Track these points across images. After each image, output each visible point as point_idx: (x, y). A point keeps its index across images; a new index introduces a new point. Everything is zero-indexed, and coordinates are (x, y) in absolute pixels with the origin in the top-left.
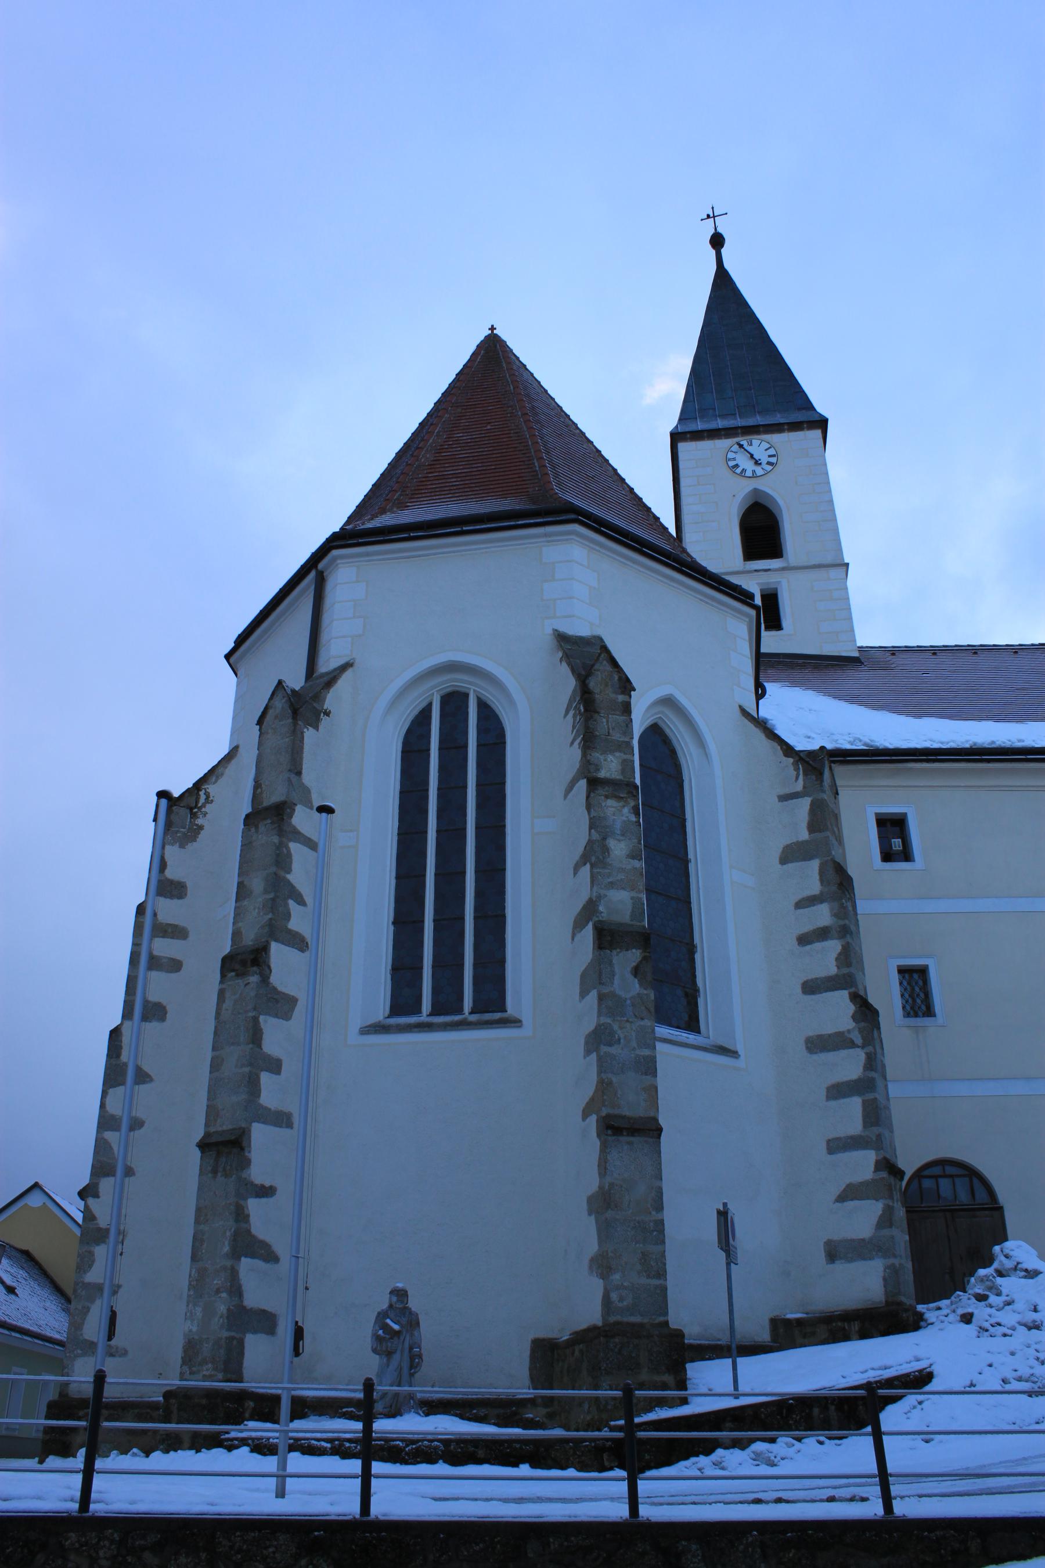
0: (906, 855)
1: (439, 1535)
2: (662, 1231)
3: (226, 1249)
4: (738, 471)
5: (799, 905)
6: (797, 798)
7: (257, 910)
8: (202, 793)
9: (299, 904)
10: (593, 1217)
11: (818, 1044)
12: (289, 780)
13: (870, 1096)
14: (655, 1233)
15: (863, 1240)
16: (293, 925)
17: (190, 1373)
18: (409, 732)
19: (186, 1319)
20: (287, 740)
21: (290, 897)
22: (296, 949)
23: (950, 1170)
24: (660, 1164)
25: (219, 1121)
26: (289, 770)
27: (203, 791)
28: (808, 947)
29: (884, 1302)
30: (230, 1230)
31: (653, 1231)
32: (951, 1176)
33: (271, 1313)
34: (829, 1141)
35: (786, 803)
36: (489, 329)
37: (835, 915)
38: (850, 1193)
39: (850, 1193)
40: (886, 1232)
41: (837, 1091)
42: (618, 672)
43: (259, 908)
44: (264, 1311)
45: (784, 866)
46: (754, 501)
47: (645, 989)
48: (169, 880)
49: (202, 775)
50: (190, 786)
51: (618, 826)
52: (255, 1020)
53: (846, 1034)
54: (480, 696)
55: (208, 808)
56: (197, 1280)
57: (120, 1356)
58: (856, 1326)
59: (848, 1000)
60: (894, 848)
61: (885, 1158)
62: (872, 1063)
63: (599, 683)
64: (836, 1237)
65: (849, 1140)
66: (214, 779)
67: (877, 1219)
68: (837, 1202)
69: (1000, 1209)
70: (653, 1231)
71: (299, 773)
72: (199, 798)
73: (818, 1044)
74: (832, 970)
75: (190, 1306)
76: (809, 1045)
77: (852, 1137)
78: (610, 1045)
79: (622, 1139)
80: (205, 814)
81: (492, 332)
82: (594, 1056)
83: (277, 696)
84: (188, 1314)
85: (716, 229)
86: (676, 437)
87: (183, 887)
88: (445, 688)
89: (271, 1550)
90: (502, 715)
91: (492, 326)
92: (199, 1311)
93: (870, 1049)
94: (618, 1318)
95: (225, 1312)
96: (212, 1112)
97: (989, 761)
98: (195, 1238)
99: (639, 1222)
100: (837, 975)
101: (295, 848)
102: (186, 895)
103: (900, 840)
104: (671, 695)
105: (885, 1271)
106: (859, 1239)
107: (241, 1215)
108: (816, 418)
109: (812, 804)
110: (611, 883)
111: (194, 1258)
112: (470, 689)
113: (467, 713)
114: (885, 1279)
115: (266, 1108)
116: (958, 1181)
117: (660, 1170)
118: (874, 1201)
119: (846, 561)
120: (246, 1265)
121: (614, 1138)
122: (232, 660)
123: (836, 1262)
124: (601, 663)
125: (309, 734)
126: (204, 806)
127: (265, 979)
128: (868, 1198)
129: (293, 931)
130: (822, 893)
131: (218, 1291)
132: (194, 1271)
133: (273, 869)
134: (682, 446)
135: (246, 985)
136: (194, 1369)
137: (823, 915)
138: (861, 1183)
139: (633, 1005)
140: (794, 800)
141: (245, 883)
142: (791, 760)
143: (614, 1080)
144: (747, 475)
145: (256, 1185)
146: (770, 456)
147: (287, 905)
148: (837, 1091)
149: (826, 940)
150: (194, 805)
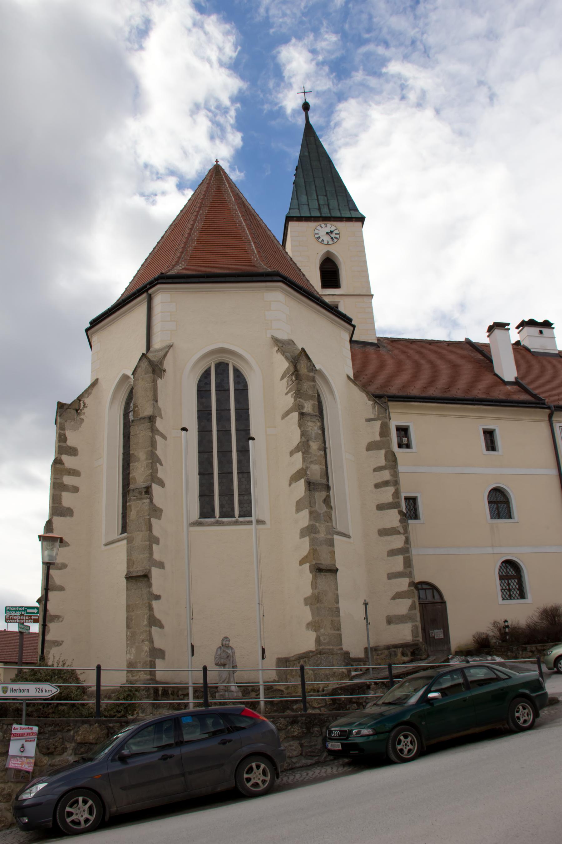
0: (408, 446)
2: (339, 612)
3: (145, 623)
4: (320, 240)
5: (375, 470)
6: (374, 421)
7: (143, 468)
8: (81, 402)
11: (383, 532)
12: (154, 405)
13: (407, 555)
15: (403, 615)
17: (132, 676)
18: (200, 381)
19: (127, 654)
20: (150, 384)
23: (425, 586)
24: (337, 584)
25: (134, 566)
26: (153, 400)
27: (82, 401)
28: (379, 489)
30: (147, 614)
31: (335, 612)
32: (425, 589)
34: (388, 574)
35: (369, 422)
36: (215, 161)
37: (392, 476)
38: (398, 596)
39: (398, 596)
40: (413, 612)
41: (392, 553)
42: (310, 361)
43: (144, 467)
44: (161, 649)
45: (369, 452)
46: (327, 257)
47: (328, 509)
49: (81, 393)
50: (75, 398)
51: (313, 435)
52: (149, 520)
54: (234, 365)
55: (85, 410)
56: (131, 637)
58: (400, 650)
59: (397, 514)
60: (404, 442)
61: (413, 581)
62: (407, 541)
63: (303, 369)
64: (391, 614)
66: (87, 395)
69: (443, 603)
70: (335, 612)
71: (157, 401)
72: (80, 405)
73: (383, 532)
74: (390, 500)
75: (129, 648)
76: (380, 533)
77: (399, 573)
78: (315, 533)
79: (322, 573)
80: (84, 413)
81: (217, 163)
82: (307, 539)
83: (142, 361)
84: (128, 651)
85: (305, 100)
86: (289, 219)
87: (76, 450)
88: (216, 360)
89: (279, 724)
90: (246, 374)
91: (217, 160)
92: (133, 650)
93: (406, 535)
94: (323, 647)
95: (148, 650)
96: (130, 562)
97: (447, 403)
98: (127, 618)
99: (330, 608)
100: (392, 502)
101: (158, 438)
102: (78, 454)
104: (320, 369)
105: (412, 627)
106: (401, 615)
107: (151, 608)
108: (360, 216)
109: (382, 424)
110: (312, 461)
111: (128, 627)
112: (230, 361)
113: (228, 374)
114: (412, 631)
116: (427, 591)
117: (337, 586)
118: (408, 599)
119: (372, 293)
120: (154, 629)
121: (319, 573)
122: (89, 332)
124: (302, 357)
125: (159, 381)
127: (151, 500)
128: (405, 598)
130: (386, 465)
131: (143, 641)
133: (150, 448)
134: (291, 224)
136: (134, 674)
137: (386, 475)
138: (403, 592)
139: (324, 516)
140: (373, 422)
141: (135, 454)
142: (371, 403)
143: (318, 548)
144: (324, 243)
147: (156, 466)
148: (392, 553)
150: (78, 409)
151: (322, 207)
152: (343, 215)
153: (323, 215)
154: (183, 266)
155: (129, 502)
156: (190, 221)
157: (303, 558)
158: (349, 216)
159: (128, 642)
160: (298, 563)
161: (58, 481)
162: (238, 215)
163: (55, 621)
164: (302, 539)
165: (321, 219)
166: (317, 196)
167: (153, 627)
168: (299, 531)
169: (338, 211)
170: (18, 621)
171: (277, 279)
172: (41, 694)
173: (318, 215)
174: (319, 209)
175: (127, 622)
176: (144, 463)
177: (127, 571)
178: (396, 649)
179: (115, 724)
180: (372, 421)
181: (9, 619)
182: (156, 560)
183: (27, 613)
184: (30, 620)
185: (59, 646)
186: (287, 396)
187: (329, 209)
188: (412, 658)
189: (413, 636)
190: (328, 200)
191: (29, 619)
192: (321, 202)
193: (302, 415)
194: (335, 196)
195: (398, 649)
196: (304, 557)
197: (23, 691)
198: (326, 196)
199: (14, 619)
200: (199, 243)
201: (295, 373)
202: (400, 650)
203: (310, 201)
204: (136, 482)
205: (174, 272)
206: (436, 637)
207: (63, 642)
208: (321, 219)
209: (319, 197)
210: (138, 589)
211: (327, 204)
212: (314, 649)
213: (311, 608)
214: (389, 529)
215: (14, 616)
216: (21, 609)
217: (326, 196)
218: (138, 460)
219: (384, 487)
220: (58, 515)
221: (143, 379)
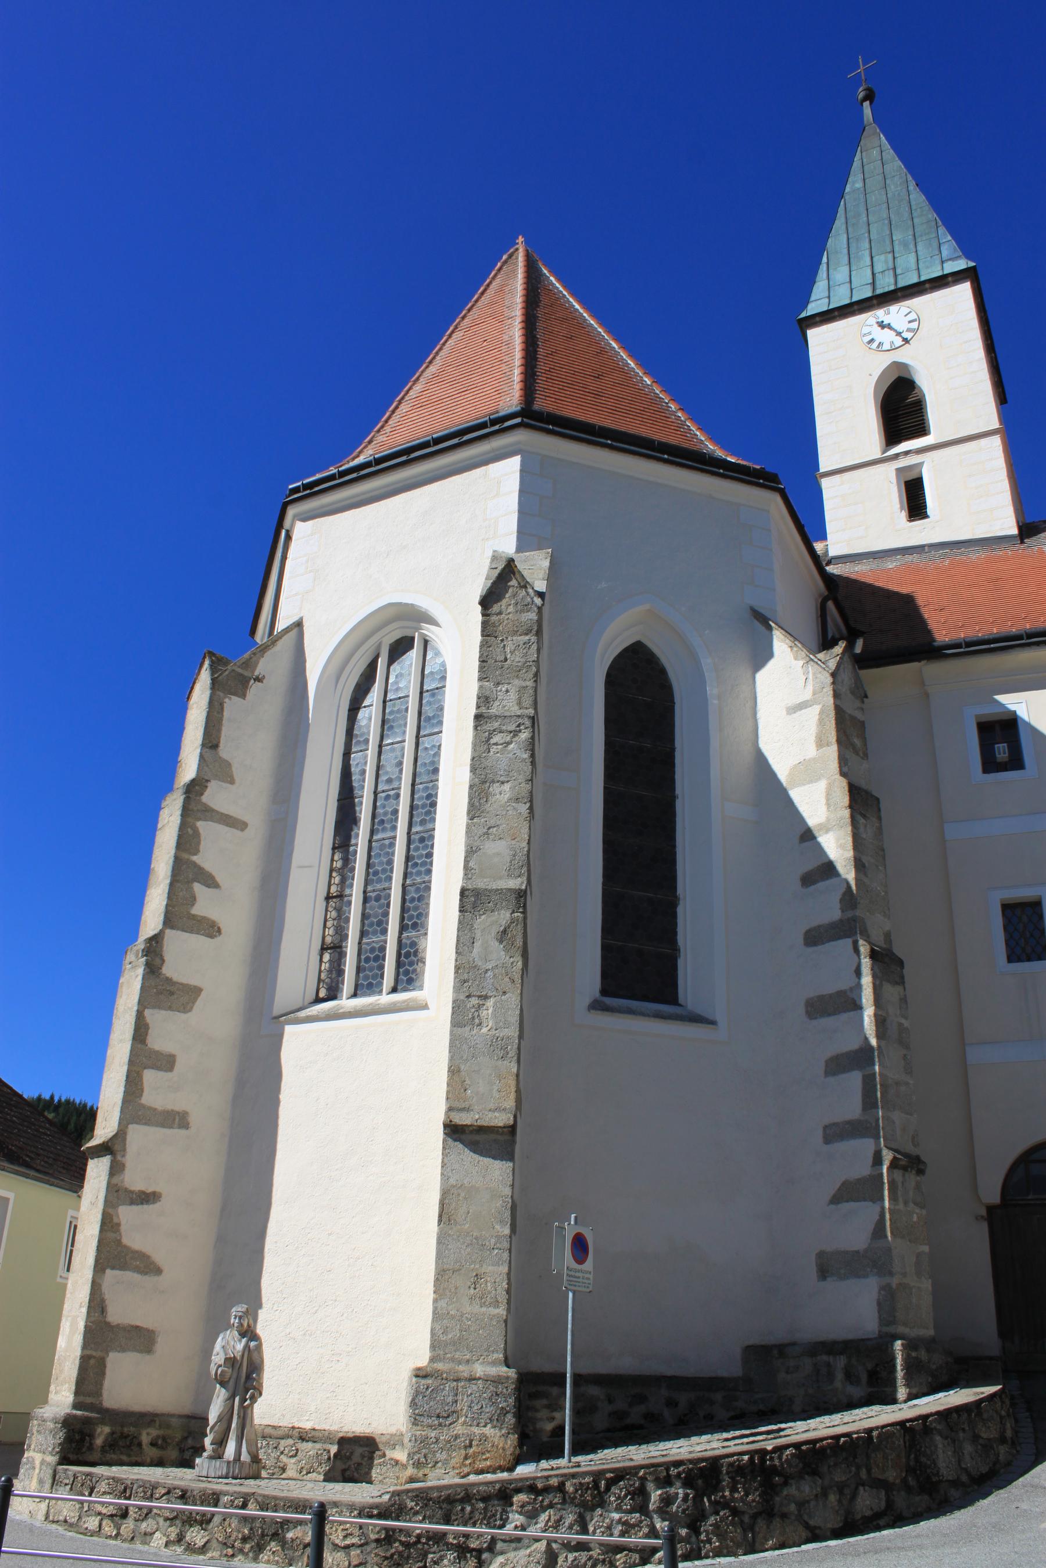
1: (759, 1476)
4: (874, 345)
9: (208, 886)
14: (496, 1251)
15: (858, 1252)
16: (197, 910)
21: (196, 879)
22: (203, 935)
28: (812, 888)
29: (877, 1333)
33: (148, 1330)
34: (826, 1128)
53: (848, 993)
60: (997, 756)
65: (847, 1126)
67: (873, 1226)
68: (832, 1204)
100: (841, 921)
103: (1005, 745)
105: (879, 1293)
106: (852, 1251)
114: (879, 1304)
115: (150, 1108)
123: (829, 1279)
129: (197, 916)
130: (828, 820)
138: (859, 1180)
145: (132, 1192)
146: (910, 322)
149: (831, 878)
167: (108, 1271)
178: (831, 1359)
180: (801, 709)
188: (870, 1390)
195: (838, 1357)
202: (841, 1362)
208: (875, 302)
214: (831, 996)
219: (823, 879)
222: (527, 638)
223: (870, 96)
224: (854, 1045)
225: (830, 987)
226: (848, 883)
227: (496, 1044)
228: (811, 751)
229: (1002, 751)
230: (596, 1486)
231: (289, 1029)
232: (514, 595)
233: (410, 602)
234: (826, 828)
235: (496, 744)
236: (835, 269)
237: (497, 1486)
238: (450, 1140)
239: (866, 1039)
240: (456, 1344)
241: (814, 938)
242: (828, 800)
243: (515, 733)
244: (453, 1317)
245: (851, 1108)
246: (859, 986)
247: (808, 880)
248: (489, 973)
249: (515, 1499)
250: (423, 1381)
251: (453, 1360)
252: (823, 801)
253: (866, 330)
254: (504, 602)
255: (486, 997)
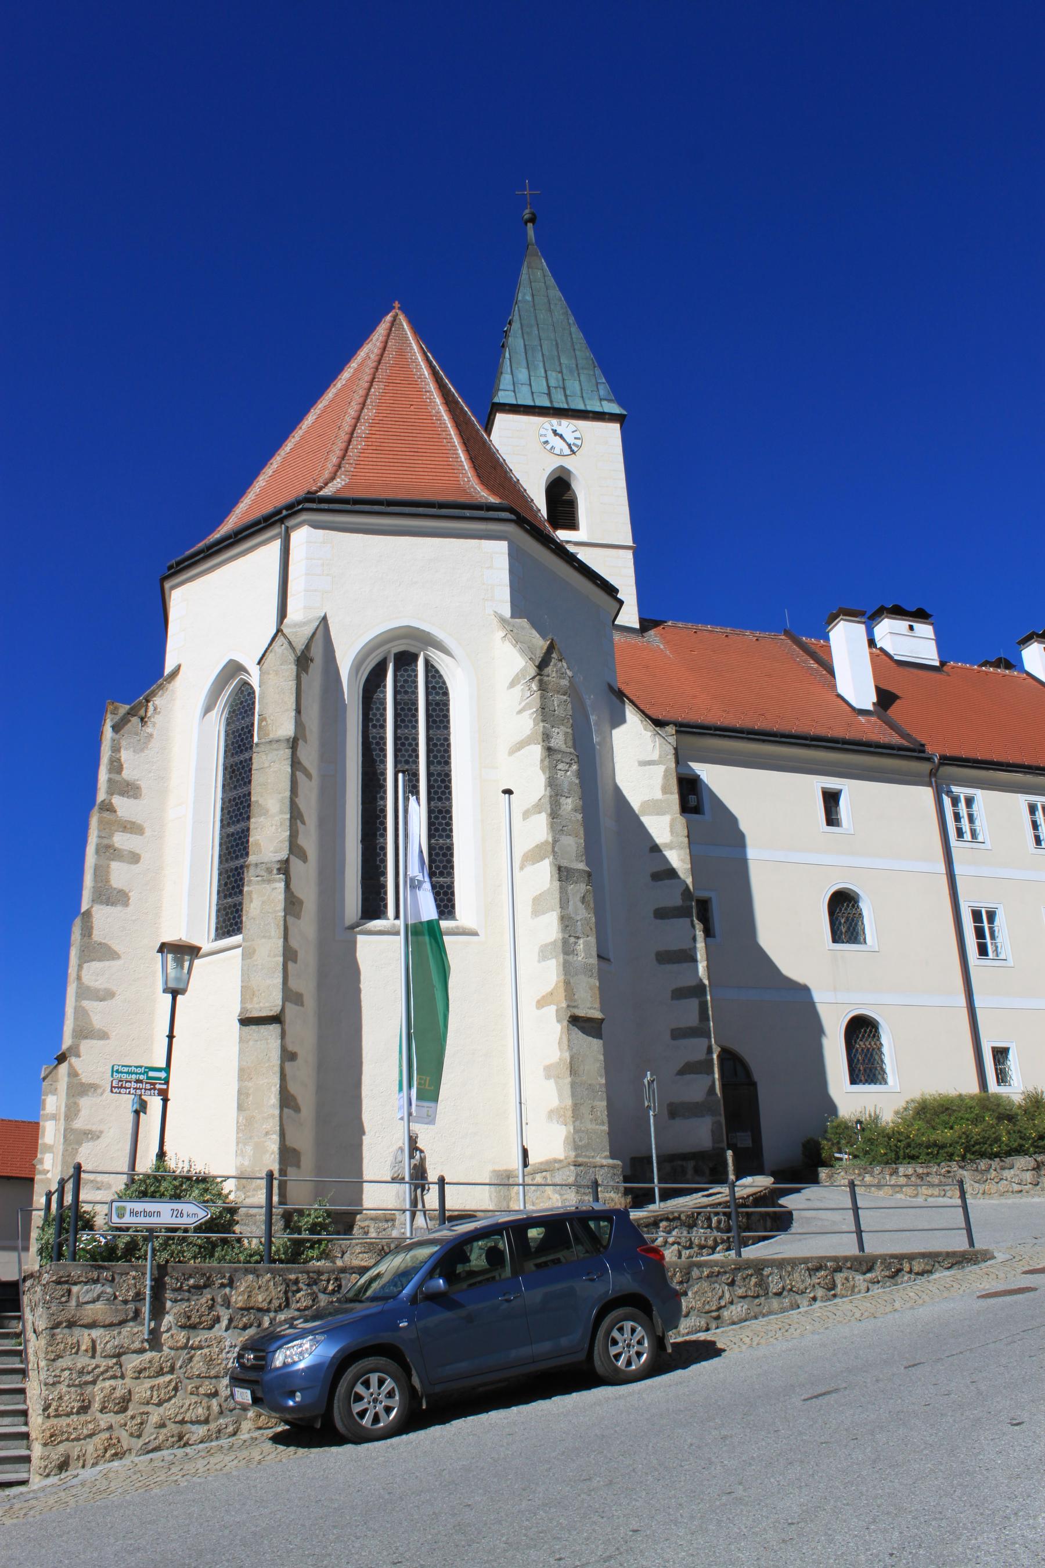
4: (548, 447)
7: (274, 827)
8: (150, 705)
10: (552, 1081)
15: (697, 1103)
28: (660, 883)
34: (673, 1031)
48: (125, 781)
51: (566, 785)
57: (105, 1190)
58: (690, 1165)
69: (754, 1084)
75: (240, 1145)
77: (690, 1028)
80: (154, 724)
92: (249, 1150)
98: (240, 1092)
111: (240, 1108)
126: (153, 716)
130: (672, 842)
131: (267, 1134)
132: (241, 1118)
135: (273, 889)
146: (575, 438)
147: (296, 824)
151: (553, 390)
152: (589, 408)
153: (556, 405)
154: (343, 483)
155: (248, 885)
156: (352, 404)
157: (543, 997)
158: (598, 409)
159: (240, 1135)
160: (534, 1003)
161: (105, 842)
162: (435, 402)
163: (90, 1094)
164: (543, 963)
165: (551, 411)
166: (546, 371)
168: (537, 949)
169: (581, 399)
170: (132, 1091)
171: (506, 517)
172: (179, 1220)
173: (547, 404)
174: (549, 394)
175: (238, 1099)
176: (277, 818)
177: (241, 1008)
178: (684, 1163)
179: (300, 1275)
180: (650, 765)
181: (118, 1088)
182: (292, 991)
183: (149, 1078)
184: (152, 1091)
185: (96, 1139)
186: (519, 716)
187: (566, 396)
189: (714, 1141)
190: (563, 380)
191: (150, 1090)
192: (552, 383)
193: (550, 750)
194: (576, 375)
196: (547, 994)
197: (150, 1214)
198: (561, 372)
199: (126, 1088)
200: (370, 444)
201: (537, 678)
203: (532, 378)
204: (261, 852)
205: (327, 492)
206: (739, 1145)
207: (101, 1132)
208: (551, 411)
209: (549, 373)
210: (261, 1040)
211: (562, 386)
212: (562, 1157)
213: (556, 1083)
215: (127, 1082)
216: (139, 1070)
217: (561, 372)
218: (266, 812)
220: (101, 903)
221: (277, 673)
222: (565, 697)
223: (532, 220)
224: (693, 983)
225: (675, 946)
226: (687, 885)
227: (587, 969)
228: (658, 795)
229: (692, 800)
230: (693, 1217)
231: (361, 939)
232: (555, 665)
233: (427, 630)
234: (670, 846)
235: (560, 770)
236: (517, 368)
237: (652, 1219)
238: (571, 1026)
239: (701, 980)
240: (587, 1147)
241: (661, 914)
242: (671, 829)
243: (570, 765)
244: (583, 1131)
245: (692, 1019)
246: (695, 948)
247: (656, 877)
248: (579, 923)
249: (661, 1225)
250: (579, 1168)
251: (586, 1156)
252: (668, 829)
253: (542, 432)
254: (550, 668)
255: (578, 938)
